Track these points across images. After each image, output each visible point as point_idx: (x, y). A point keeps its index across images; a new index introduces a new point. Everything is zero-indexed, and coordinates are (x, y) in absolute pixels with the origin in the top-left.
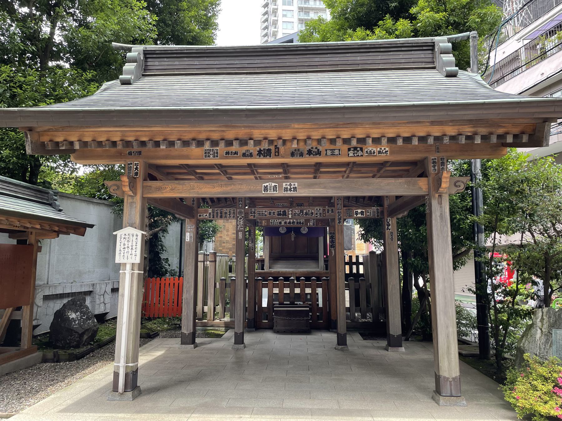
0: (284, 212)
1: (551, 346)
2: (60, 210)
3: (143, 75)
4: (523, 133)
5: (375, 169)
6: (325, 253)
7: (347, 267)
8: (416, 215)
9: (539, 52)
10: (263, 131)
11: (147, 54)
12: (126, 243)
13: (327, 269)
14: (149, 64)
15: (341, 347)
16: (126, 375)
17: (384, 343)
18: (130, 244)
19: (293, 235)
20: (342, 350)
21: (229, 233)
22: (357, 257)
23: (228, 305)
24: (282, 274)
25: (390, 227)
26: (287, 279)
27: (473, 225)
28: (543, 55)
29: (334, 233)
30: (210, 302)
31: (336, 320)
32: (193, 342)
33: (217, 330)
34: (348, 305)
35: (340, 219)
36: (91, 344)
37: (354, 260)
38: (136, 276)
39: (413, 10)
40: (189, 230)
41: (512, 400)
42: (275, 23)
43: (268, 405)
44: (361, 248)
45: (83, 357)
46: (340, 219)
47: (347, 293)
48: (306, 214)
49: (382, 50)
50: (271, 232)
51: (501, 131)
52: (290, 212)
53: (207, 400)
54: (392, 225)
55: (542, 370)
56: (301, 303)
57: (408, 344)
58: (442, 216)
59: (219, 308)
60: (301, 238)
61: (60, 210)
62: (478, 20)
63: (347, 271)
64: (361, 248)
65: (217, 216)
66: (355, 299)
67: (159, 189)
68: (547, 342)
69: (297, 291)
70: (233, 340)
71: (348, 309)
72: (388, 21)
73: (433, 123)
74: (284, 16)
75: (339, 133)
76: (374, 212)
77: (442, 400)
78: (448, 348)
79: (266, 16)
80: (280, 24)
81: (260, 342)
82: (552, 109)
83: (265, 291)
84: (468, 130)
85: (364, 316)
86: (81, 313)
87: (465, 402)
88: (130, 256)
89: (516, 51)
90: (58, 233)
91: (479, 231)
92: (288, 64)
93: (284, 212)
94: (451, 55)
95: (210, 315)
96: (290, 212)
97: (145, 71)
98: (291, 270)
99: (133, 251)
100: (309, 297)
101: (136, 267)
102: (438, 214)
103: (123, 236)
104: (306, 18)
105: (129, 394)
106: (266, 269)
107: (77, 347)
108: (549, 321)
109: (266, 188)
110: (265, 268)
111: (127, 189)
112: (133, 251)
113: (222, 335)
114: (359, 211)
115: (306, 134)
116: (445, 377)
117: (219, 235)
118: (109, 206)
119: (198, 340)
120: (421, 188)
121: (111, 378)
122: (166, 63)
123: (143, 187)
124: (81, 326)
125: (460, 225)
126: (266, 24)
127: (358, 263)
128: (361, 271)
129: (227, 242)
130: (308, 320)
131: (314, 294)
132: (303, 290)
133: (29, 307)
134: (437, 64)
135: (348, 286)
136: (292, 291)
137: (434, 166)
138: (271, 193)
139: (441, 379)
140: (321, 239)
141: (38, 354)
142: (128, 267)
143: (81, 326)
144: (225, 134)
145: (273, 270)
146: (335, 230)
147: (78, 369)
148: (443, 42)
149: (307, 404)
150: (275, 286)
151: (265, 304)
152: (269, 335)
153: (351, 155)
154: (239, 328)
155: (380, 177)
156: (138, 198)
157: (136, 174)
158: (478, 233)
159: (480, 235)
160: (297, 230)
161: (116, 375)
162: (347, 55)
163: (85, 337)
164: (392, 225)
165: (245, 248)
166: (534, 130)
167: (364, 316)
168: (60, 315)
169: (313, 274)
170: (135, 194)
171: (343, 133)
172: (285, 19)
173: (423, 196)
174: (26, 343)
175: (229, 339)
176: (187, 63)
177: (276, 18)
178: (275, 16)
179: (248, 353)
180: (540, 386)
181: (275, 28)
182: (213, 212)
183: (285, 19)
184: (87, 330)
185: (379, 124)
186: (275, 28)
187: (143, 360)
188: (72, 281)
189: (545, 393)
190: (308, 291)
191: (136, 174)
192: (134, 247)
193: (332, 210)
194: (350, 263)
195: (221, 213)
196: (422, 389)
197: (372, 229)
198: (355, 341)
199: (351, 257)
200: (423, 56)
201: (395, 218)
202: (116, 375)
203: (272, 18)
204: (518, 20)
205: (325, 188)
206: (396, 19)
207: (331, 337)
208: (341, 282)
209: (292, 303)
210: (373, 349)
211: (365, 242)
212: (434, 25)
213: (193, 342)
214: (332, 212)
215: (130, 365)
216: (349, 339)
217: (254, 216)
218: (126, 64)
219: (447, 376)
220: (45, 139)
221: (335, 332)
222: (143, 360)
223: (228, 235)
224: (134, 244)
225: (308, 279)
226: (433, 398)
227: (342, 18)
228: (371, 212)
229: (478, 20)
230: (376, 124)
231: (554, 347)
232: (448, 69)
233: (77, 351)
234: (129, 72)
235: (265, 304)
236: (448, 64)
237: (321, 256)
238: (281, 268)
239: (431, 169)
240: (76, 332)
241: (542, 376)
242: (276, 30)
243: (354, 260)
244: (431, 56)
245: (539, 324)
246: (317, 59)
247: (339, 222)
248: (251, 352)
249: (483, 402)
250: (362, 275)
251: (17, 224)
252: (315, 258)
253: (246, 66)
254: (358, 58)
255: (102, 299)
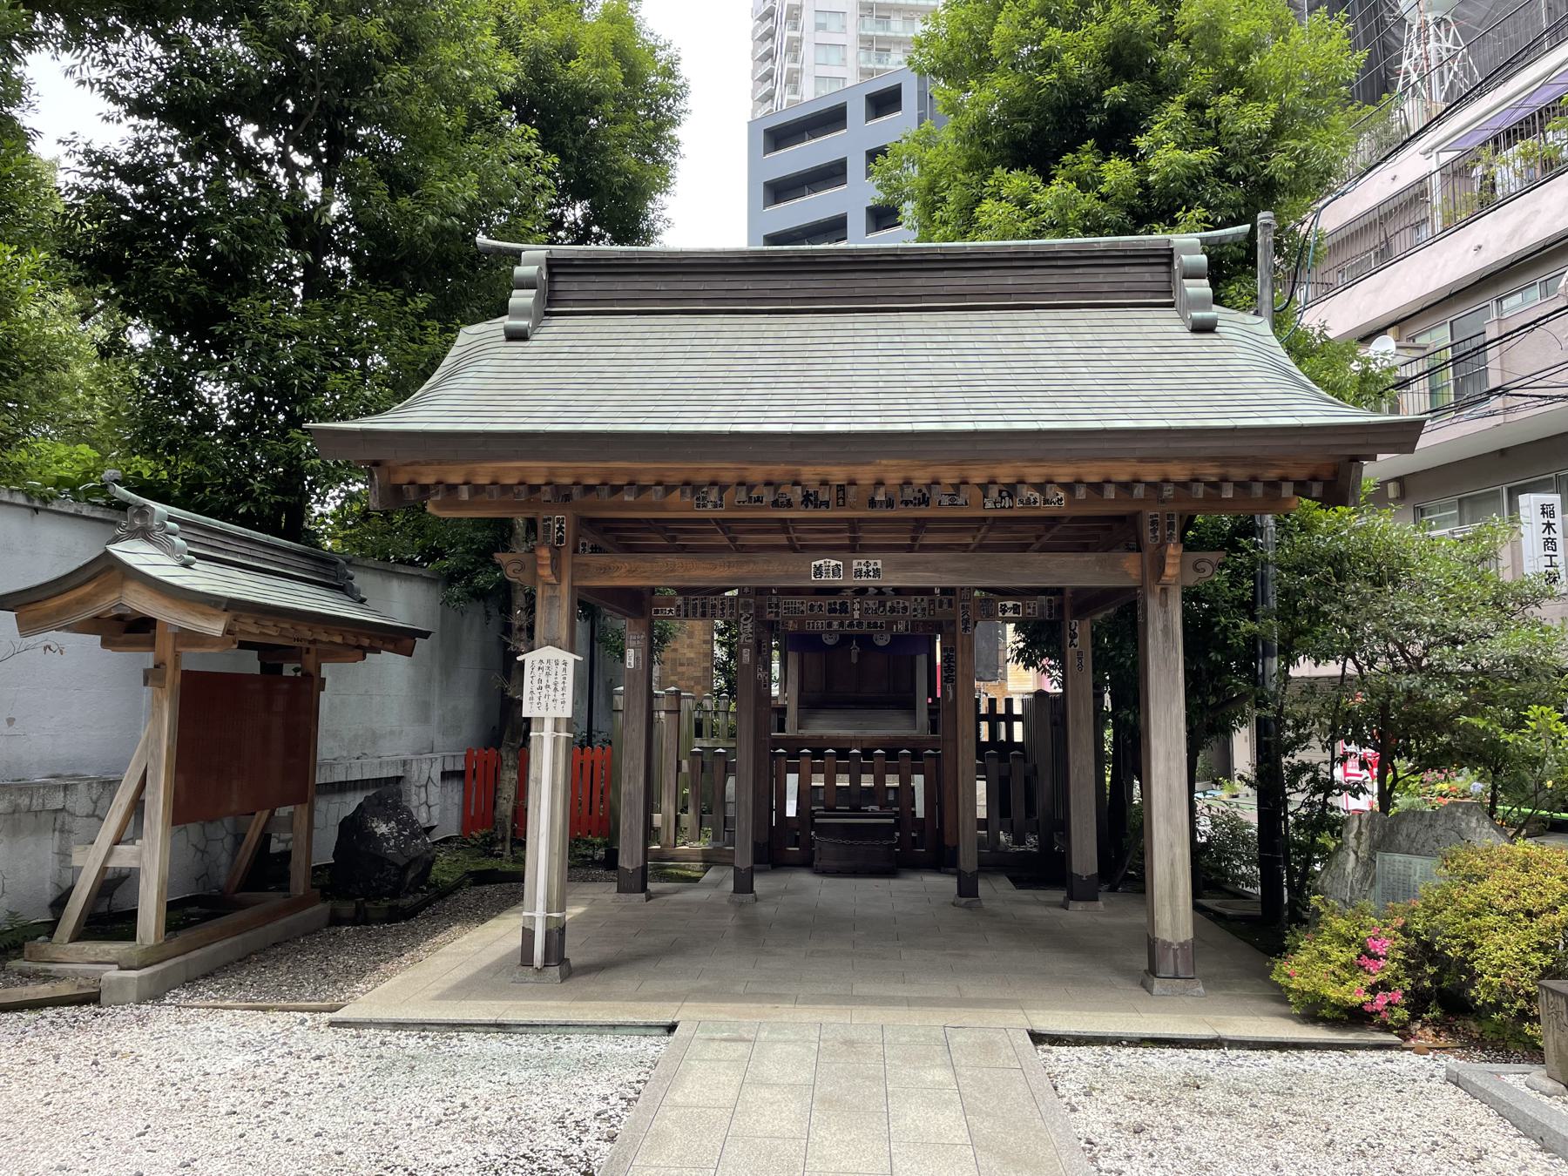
0: (843, 604)
1: (1372, 885)
2: (362, 601)
3: (547, 314)
4: (1314, 479)
5: (1042, 527)
6: (931, 692)
7: (984, 726)
8: (1122, 622)
9: (1476, 187)
10: (820, 469)
11: (554, 266)
12: (544, 679)
13: (934, 731)
14: (558, 287)
15: (964, 900)
16: (548, 934)
17: (1060, 895)
18: (552, 680)
19: (855, 650)
20: (968, 906)
21: (696, 641)
22: (1009, 702)
23: (710, 807)
24: (831, 742)
25: (1076, 641)
26: (843, 753)
27: (1252, 640)
28: (1489, 200)
29: (952, 650)
30: (668, 805)
31: (956, 848)
32: (644, 889)
33: (683, 868)
34: (982, 813)
35: (966, 622)
36: (422, 891)
37: (1001, 709)
38: (562, 742)
39: (1142, 142)
40: (632, 643)
41: (1282, 980)
42: (794, 47)
43: (824, 991)
44: (1020, 683)
45: (415, 915)
46: (966, 622)
47: (981, 787)
48: (892, 610)
49: (1060, 263)
50: (802, 643)
51: (1272, 474)
52: (857, 606)
53: (704, 982)
54: (1080, 633)
55: (1340, 925)
56: (876, 808)
57: (1113, 897)
58: (1166, 630)
59: (688, 819)
60: (874, 663)
61: (362, 601)
62: (1292, 164)
63: (985, 737)
64: (1020, 683)
65: (694, 614)
66: (999, 798)
67: (605, 570)
68: (1365, 878)
69: (867, 781)
70: (730, 885)
71: (982, 824)
72: (1085, 159)
73: (1142, 460)
74: (820, 27)
75: (965, 473)
76: (1041, 607)
77: (1157, 985)
78: (1173, 886)
79: (768, 24)
80: (807, 50)
81: (786, 891)
82: (1359, 440)
83: (792, 780)
84: (1211, 472)
85: (1019, 840)
86: (398, 823)
87: (1201, 989)
88: (551, 704)
89: (1420, 182)
90: (362, 651)
91: (1268, 653)
92: (858, 292)
93: (843, 604)
94: (1206, 281)
95: (668, 833)
96: (857, 606)
97: (551, 304)
98: (850, 733)
99: (559, 694)
100: (891, 797)
101: (563, 726)
102: (1159, 626)
103: (537, 665)
104: (881, 33)
105: (555, 971)
106: (791, 730)
107: (394, 894)
108: (1371, 837)
109: (818, 568)
110: (787, 726)
111: (546, 572)
112: (559, 694)
113: (697, 880)
114: (1010, 604)
115: (901, 475)
116: (1164, 942)
117: (671, 644)
118: (430, 581)
119: (652, 886)
120: (1127, 574)
121: (516, 941)
122: (595, 285)
123: (573, 565)
124: (401, 851)
125: (1227, 638)
126: (768, 45)
127: (1010, 718)
128: (1018, 737)
129: (690, 662)
130: (891, 847)
131: (906, 790)
132: (880, 780)
133: (306, 807)
134: (1176, 298)
135: (982, 770)
136: (855, 780)
137: (1154, 531)
138: (828, 580)
139: (1158, 945)
140: (922, 660)
141: (321, 909)
142: (549, 725)
143: (401, 851)
144: (747, 473)
145: (806, 733)
146: (954, 643)
147: (416, 940)
148: (1189, 250)
149: (900, 991)
150: (816, 769)
151: (791, 811)
152: (804, 879)
153: (989, 505)
154: (744, 859)
155: (1042, 550)
156: (565, 588)
157: (560, 540)
158: (1265, 656)
159: (1268, 660)
160: (866, 641)
161: (528, 935)
162: (986, 273)
163: (411, 875)
164: (1080, 633)
165: (743, 682)
166: (1336, 474)
167: (1019, 840)
168: (352, 828)
169: (904, 742)
170: (559, 580)
171: (973, 473)
172: (822, 37)
173: (1135, 588)
174: (301, 883)
175: (716, 885)
176: (639, 286)
177: (796, 34)
178: (796, 29)
179: (765, 910)
180: (1335, 954)
181: (795, 60)
182: (686, 604)
183: (822, 37)
184: (413, 860)
185: (1041, 460)
186: (795, 60)
187: (574, 911)
188: (358, 753)
189: (1344, 966)
190: (892, 781)
191: (560, 540)
192: (560, 687)
193: (950, 602)
194: (993, 718)
195: (703, 606)
196: (1126, 972)
197: (1041, 643)
198: (996, 891)
199: (992, 702)
200: (1148, 277)
201: (1088, 621)
202: (528, 935)
203: (785, 33)
204: (1442, 82)
205: (936, 571)
206: (1105, 151)
207: (949, 883)
208: (967, 759)
209: (856, 810)
210: (1038, 905)
211: (1026, 667)
212: (1188, 178)
213: (644, 889)
214: (950, 605)
215: (555, 915)
216: (983, 887)
217: (777, 614)
218: (515, 292)
219: (1169, 939)
220: (402, 478)
221: (953, 874)
222: (574, 911)
223: (691, 646)
224: (560, 680)
225: (892, 753)
226: (1144, 985)
227: (977, 140)
228: (1036, 607)
229: (1292, 164)
230: (1036, 461)
231: (1378, 887)
232: (1197, 314)
233: (408, 901)
234: (522, 313)
235: (791, 811)
236: (1198, 303)
237: (923, 701)
238: (825, 728)
239: (1148, 536)
240: (393, 864)
241: (1339, 935)
242: (797, 66)
243: (1001, 709)
244: (1165, 277)
245: (1353, 843)
246: (921, 281)
247: (966, 629)
248: (772, 909)
249: (1239, 991)
250: (1019, 746)
251: (254, 630)
252: (906, 704)
253: (769, 294)
254: (1010, 280)
255: (423, 795)
